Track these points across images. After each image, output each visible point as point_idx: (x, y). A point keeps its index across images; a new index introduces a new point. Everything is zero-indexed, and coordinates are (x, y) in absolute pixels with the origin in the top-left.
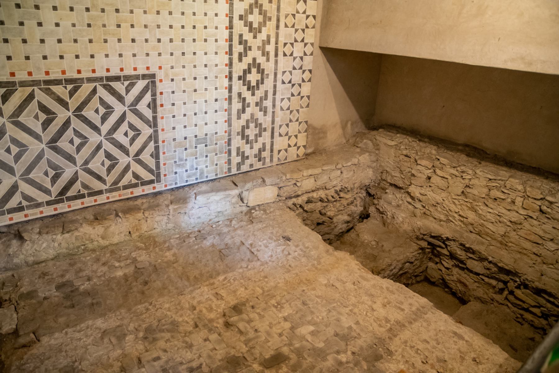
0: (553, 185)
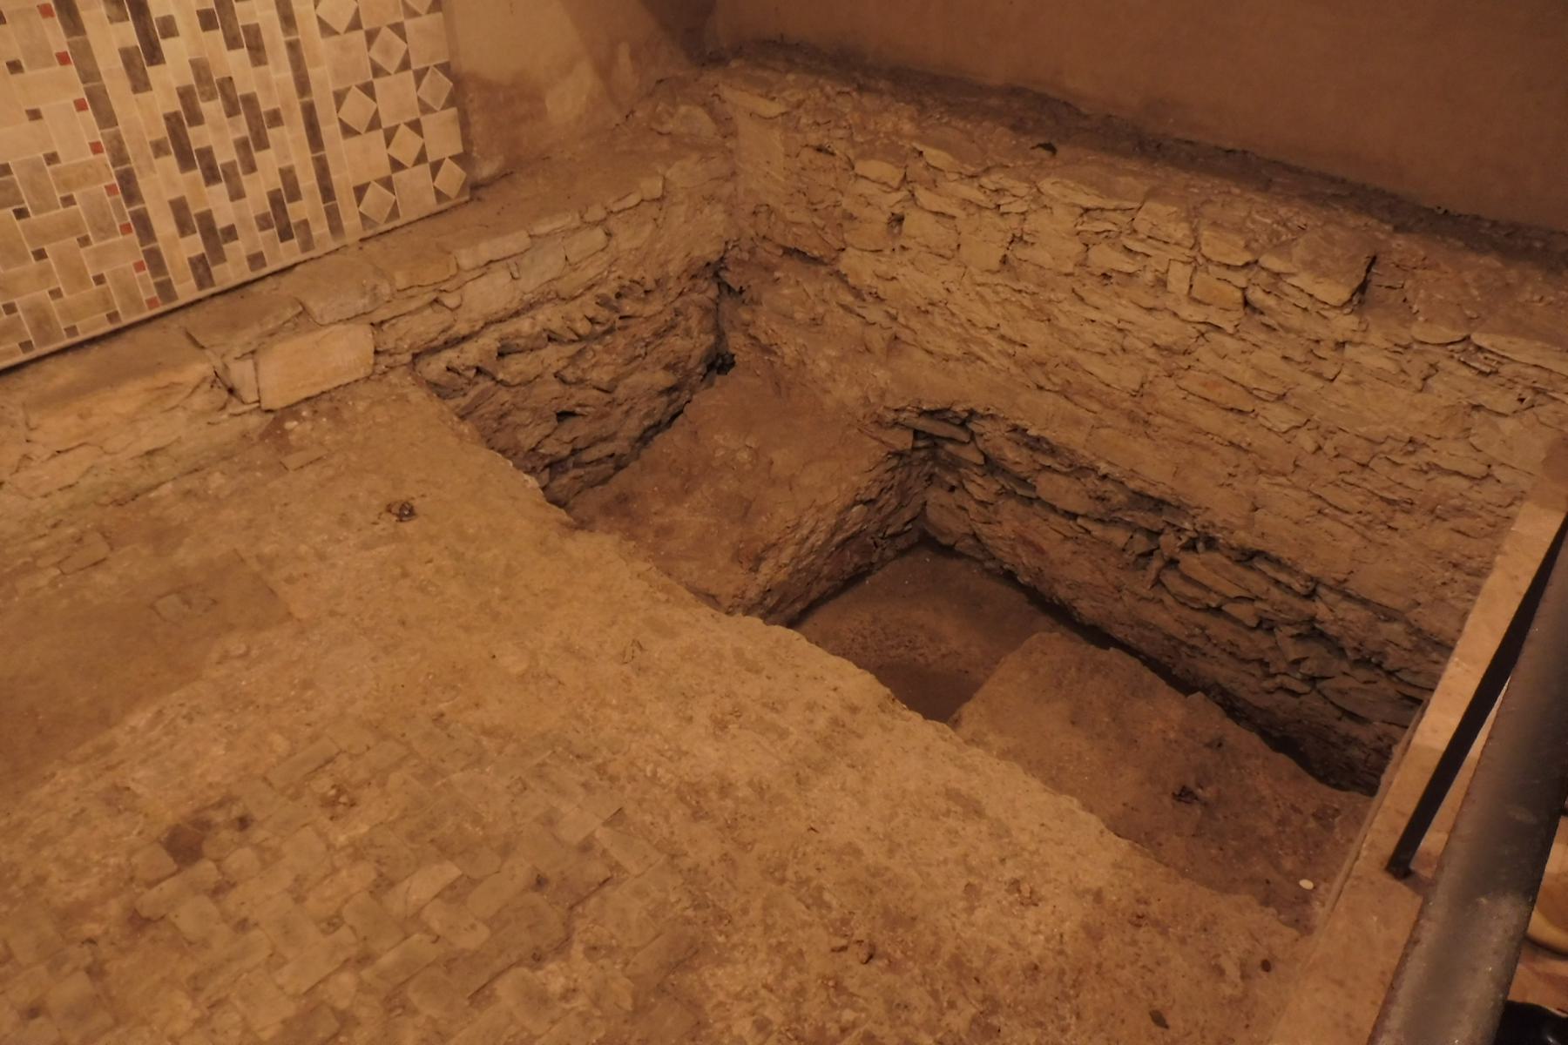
0: (1283, 211)
